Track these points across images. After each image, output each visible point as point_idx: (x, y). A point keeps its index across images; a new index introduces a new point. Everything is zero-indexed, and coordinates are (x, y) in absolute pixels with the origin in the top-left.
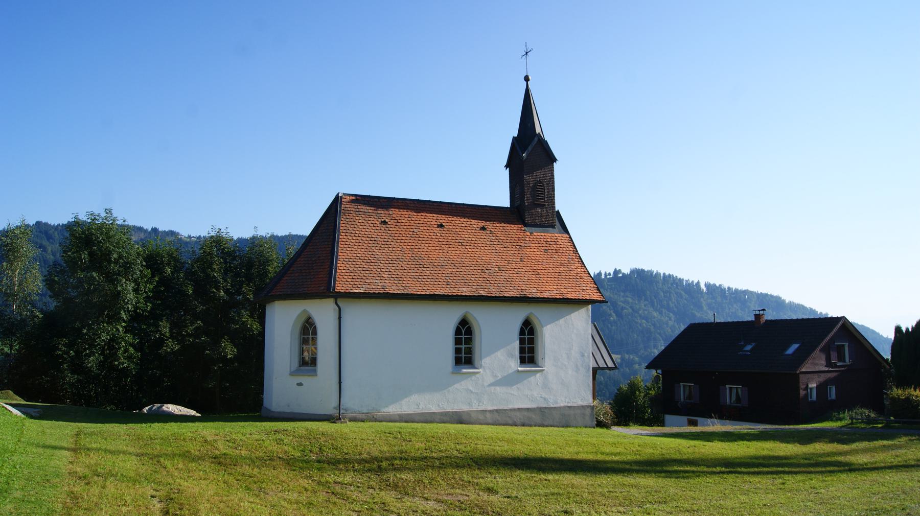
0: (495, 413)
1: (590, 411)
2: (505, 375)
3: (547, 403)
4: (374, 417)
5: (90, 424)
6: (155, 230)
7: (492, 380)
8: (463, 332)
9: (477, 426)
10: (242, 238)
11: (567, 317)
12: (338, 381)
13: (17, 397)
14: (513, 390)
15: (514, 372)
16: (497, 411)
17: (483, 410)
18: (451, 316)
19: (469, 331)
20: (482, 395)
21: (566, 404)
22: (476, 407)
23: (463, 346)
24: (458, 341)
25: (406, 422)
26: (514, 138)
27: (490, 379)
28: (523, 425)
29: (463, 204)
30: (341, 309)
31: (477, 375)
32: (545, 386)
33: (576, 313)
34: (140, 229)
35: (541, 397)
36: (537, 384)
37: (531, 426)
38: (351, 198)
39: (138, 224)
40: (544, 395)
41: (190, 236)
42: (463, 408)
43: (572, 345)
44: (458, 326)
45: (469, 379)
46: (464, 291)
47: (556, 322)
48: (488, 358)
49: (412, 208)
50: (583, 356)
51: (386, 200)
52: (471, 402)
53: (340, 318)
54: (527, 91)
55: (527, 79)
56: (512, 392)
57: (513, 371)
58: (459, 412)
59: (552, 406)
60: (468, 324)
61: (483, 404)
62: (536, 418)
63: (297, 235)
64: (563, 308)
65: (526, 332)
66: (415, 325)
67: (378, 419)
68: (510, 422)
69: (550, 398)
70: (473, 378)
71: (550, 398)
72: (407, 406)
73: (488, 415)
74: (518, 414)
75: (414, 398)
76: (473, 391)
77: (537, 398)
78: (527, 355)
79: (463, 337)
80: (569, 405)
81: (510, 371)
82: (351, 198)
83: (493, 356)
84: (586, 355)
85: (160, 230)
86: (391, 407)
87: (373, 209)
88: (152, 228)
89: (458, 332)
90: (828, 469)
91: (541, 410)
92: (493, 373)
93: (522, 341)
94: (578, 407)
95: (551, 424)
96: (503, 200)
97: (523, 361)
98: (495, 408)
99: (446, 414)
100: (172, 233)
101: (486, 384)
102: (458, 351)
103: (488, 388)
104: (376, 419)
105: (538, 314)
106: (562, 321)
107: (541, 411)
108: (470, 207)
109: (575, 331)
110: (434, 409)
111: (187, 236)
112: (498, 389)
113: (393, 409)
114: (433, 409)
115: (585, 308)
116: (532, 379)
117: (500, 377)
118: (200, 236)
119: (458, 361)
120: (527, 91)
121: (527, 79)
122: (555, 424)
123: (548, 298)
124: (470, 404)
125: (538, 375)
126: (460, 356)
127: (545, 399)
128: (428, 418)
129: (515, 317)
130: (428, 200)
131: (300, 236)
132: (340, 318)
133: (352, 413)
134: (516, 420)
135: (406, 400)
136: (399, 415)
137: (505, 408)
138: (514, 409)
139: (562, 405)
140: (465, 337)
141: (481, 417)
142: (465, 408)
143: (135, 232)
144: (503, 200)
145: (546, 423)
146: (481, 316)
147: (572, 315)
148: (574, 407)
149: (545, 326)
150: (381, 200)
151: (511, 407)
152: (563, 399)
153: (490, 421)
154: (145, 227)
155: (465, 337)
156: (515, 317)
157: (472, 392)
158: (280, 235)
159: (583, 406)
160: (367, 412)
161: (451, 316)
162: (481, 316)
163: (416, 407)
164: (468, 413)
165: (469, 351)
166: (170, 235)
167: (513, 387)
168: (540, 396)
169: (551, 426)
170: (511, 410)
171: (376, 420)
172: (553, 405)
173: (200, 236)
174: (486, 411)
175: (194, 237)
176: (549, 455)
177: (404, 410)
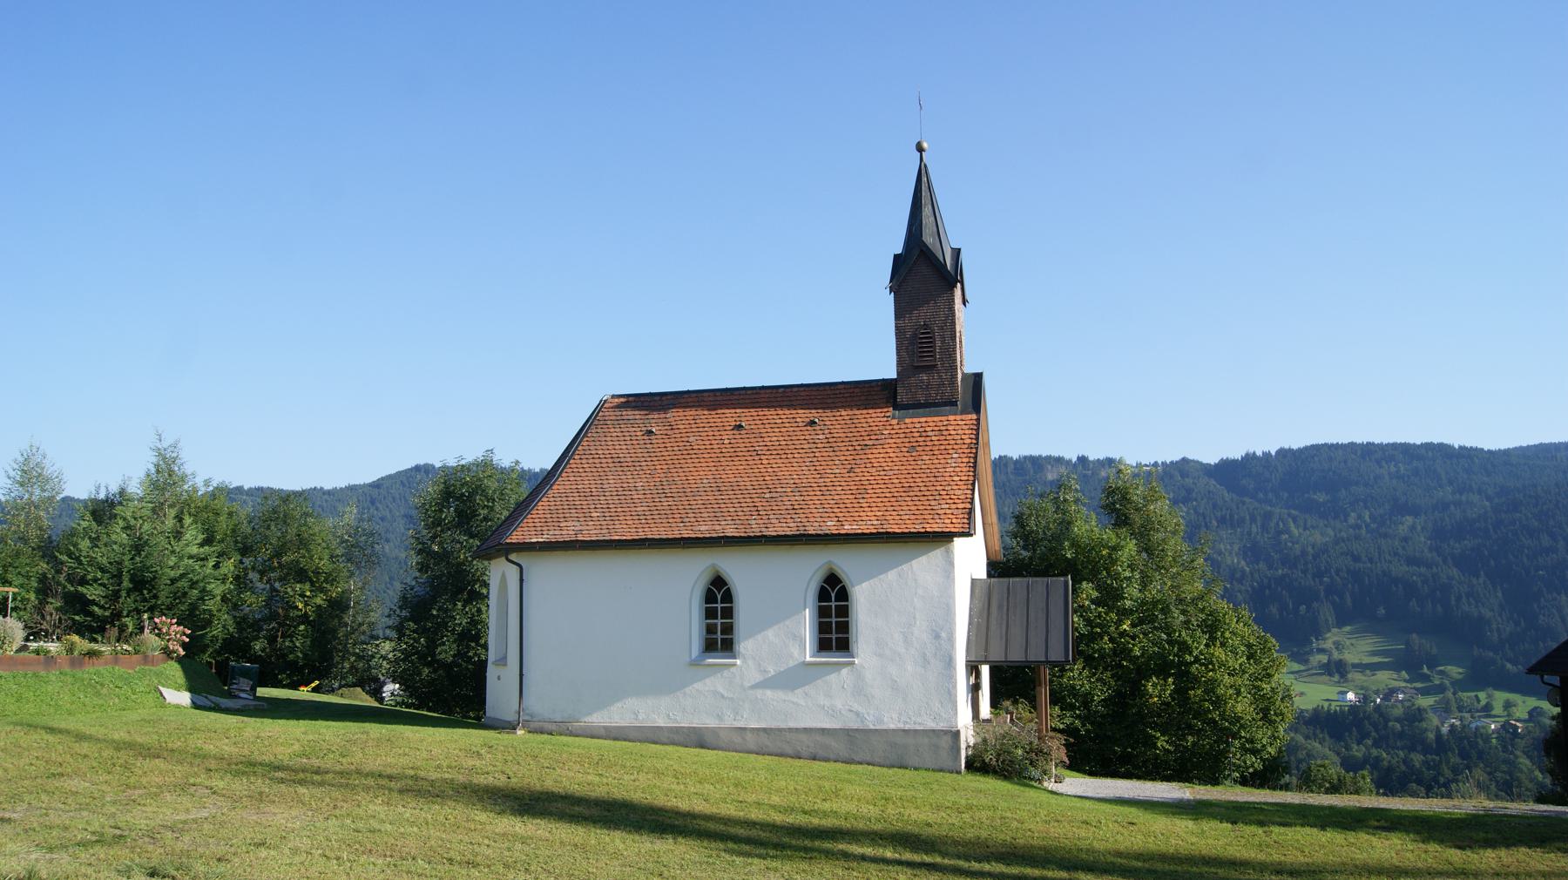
0: (761, 734)
1: (950, 743)
2: (782, 670)
3: (862, 722)
4: (568, 729)
5: (461, 730)
6: (1083, 460)
7: (759, 678)
8: (719, 597)
9: (620, 742)
10: (1227, 458)
11: (905, 567)
12: (518, 673)
13: (368, 697)
14: (797, 697)
15: (798, 664)
16: (764, 730)
17: (740, 728)
18: (690, 573)
19: (728, 597)
20: (741, 703)
21: (901, 726)
22: (730, 721)
23: (719, 621)
24: (710, 614)
25: (615, 739)
26: (897, 258)
27: (754, 676)
28: (814, 759)
29: (843, 383)
30: (524, 571)
31: (732, 669)
32: (859, 690)
33: (923, 559)
34: (1059, 460)
35: (852, 711)
36: (843, 687)
37: (827, 760)
38: (622, 400)
39: (1055, 453)
40: (856, 707)
41: (1141, 464)
42: (708, 722)
43: (914, 618)
44: (822, 586)
45: (719, 675)
46: (704, 530)
47: (882, 576)
48: (750, 641)
49: (692, 404)
50: (937, 637)
51: (849, 386)
52: (722, 713)
53: (521, 580)
54: (922, 176)
55: (920, 149)
56: (795, 700)
57: (796, 663)
58: (700, 728)
59: (872, 727)
60: (726, 584)
61: (742, 717)
62: (839, 747)
63: (1326, 444)
64: (910, 548)
65: (833, 595)
66: (631, 588)
67: (574, 731)
68: (789, 751)
69: (868, 713)
70: (726, 673)
71: (868, 713)
72: (619, 714)
73: (749, 736)
74: (803, 737)
75: (631, 703)
76: (726, 695)
77: (843, 712)
78: (834, 636)
79: (719, 606)
80: (907, 727)
81: (792, 663)
82: (622, 400)
83: (759, 637)
84: (943, 635)
85: (1091, 458)
86: (595, 715)
87: (642, 413)
88: (1078, 458)
89: (709, 597)
90: (800, 843)
91: (849, 734)
92: (760, 665)
93: (823, 612)
94: (926, 732)
95: (868, 759)
96: (884, 365)
97: (824, 646)
98: (763, 725)
99: (677, 730)
100: (1110, 462)
101: (747, 684)
102: (710, 630)
103: (751, 692)
104: (571, 731)
105: (846, 562)
106: (892, 575)
107: (849, 735)
108: (810, 389)
109: (920, 591)
110: (661, 722)
111: (1135, 465)
112: (769, 693)
113: (598, 719)
114: (660, 721)
115: (943, 549)
116: (833, 677)
117: (773, 673)
118: (1156, 462)
119: (710, 646)
120: (922, 176)
121: (920, 149)
122: (877, 760)
123: (733, 537)
124: (720, 717)
125: (845, 671)
126: (714, 637)
127: (857, 714)
128: (652, 736)
129: (806, 569)
130: (648, 392)
131: (1332, 445)
132: (521, 580)
133: (539, 721)
134: (799, 748)
135: (619, 705)
136: (605, 728)
137: (783, 726)
138: (797, 729)
139: (892, 726)
140: (723, 605)
141: (737, 739)
142: (711, 723)
143: (1052, 466)
144: (884, 365)
145: (857, 758)
146: (740, 570)
147: (914, 562)
148: (916, 731)
149: (858, 585)
150: (664, 398)
151: (792, 725)
152: (895, 716)
153: (752, 746)
154: (1067, 457)
155: (723, 605)
156: (806, 569)
157: (723, 696)
158: (1295, 447)
159: (934, 731)
160: (561, 720)
161: (690, 573)
162: (740, 570)
163: (633, 716)
164: (714, 731)
165: (728, 629)
166: (1107, 466)
167: (796, 691)
168: (847, 707)
169: (869, 764)
170: (790, 730)
171: (571, 734)
172: (874, 725)
173: (1156, 462)
174: (745, 729)
175: (1146, 465)
176: (637, 796)
177: (616, 720)
